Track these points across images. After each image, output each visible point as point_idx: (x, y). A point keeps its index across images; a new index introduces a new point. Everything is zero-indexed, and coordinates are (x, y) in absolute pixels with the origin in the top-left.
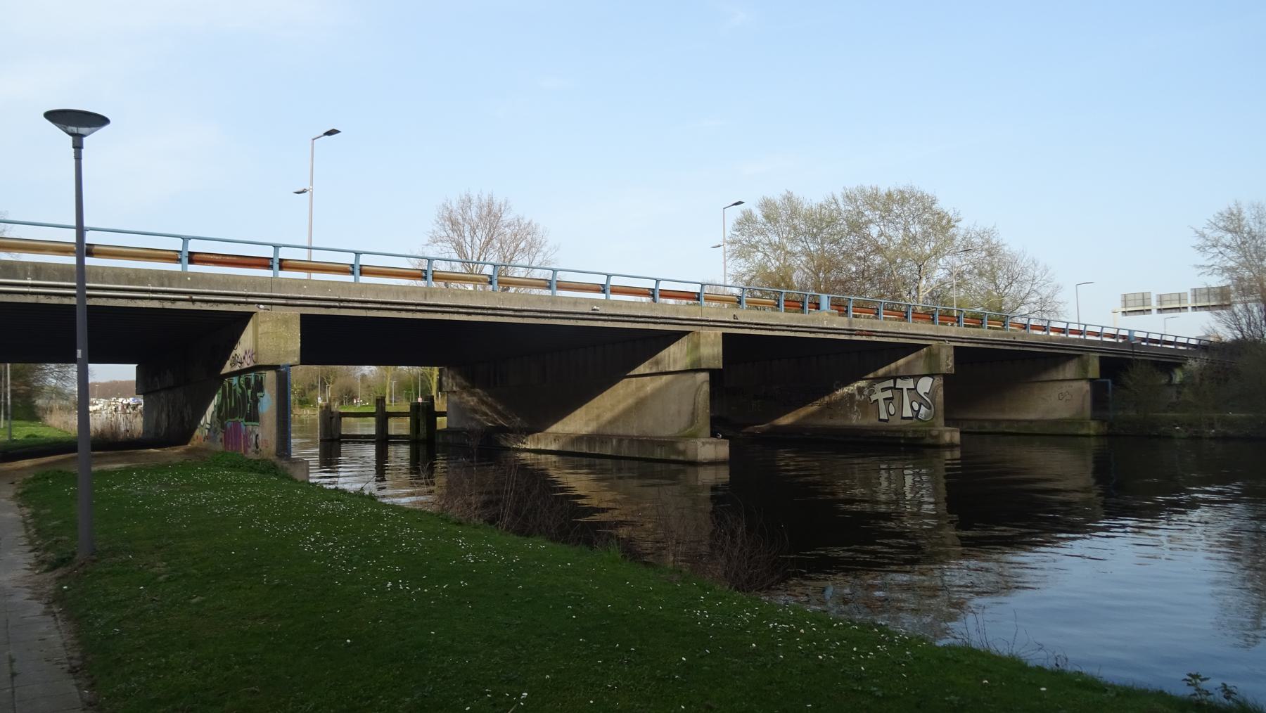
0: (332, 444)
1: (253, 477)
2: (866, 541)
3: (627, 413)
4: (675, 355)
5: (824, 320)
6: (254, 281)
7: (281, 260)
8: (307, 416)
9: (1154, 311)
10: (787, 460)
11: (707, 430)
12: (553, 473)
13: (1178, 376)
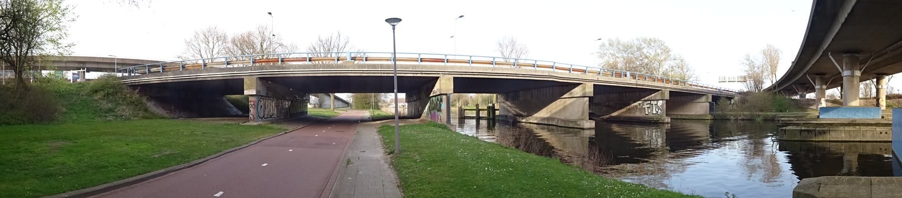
0: (462, 119)
1: (440, 130)
2: (640, 154)
3: (560, 111)
4: (577, 91)
5: (628, 81)
6: (439, 67)
8: (454, 110)
10: (615, 128)
11: (588, 118)
12: (536, 131)
13: (733, 101)
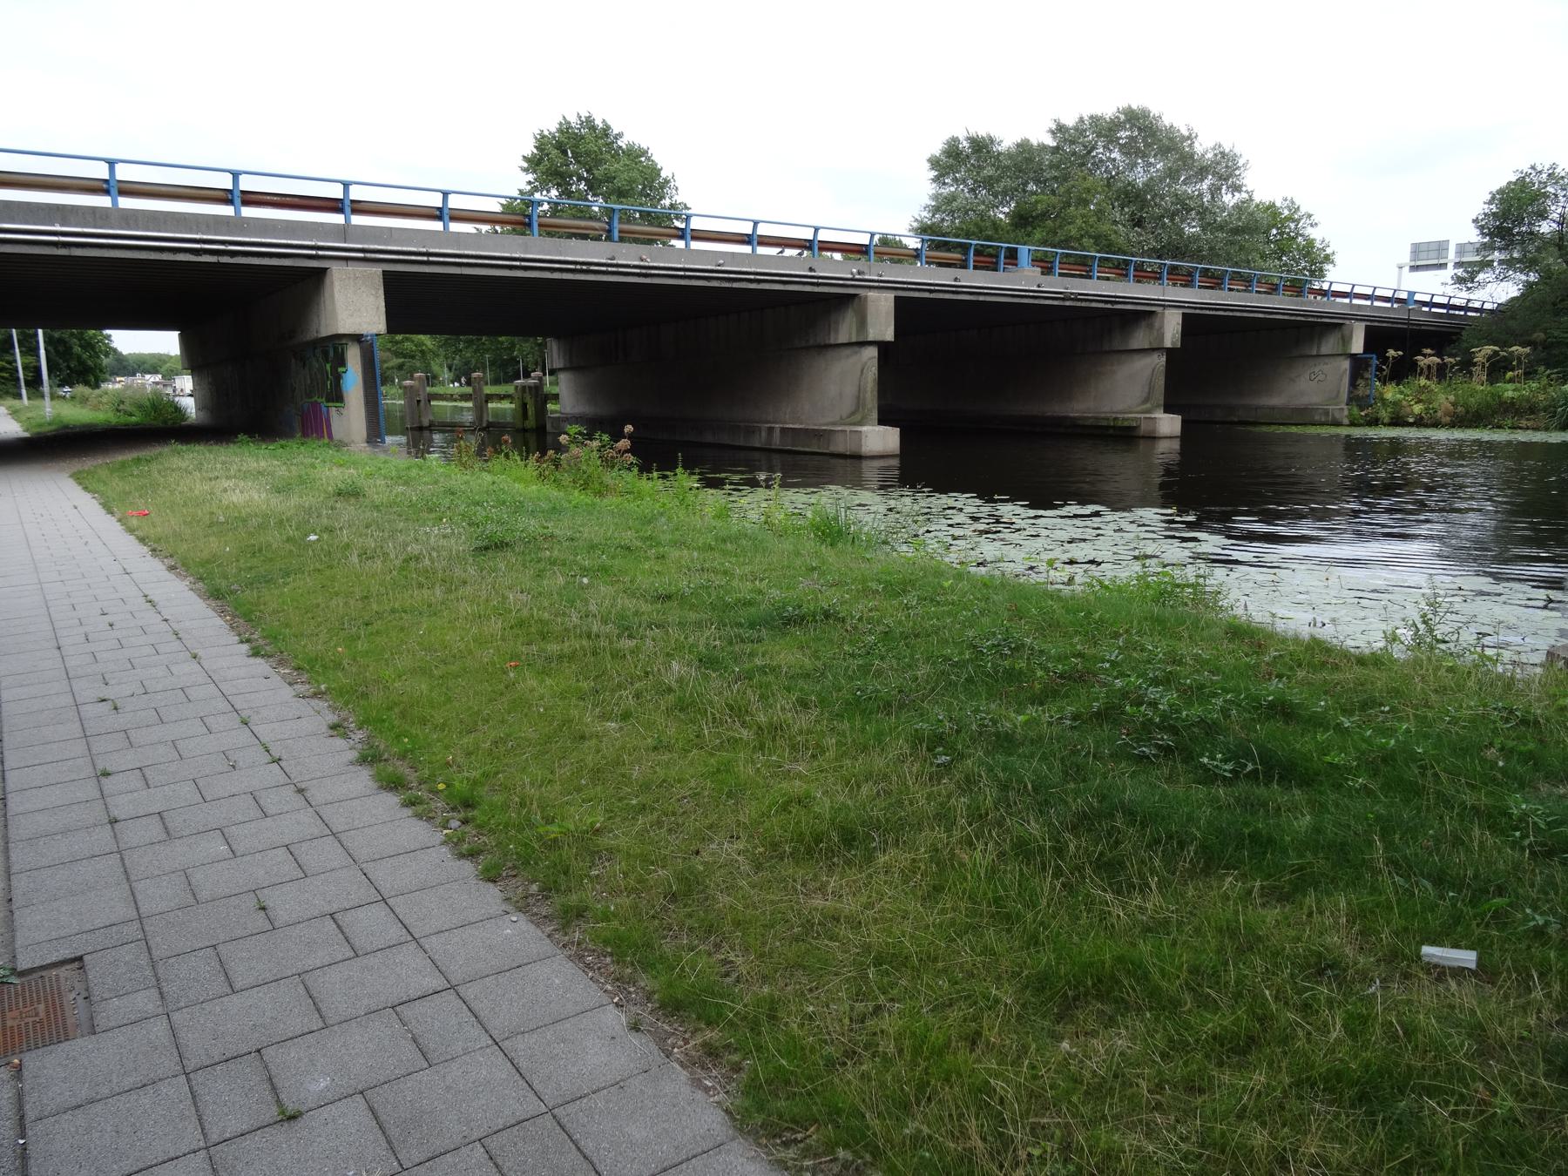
7: (353, 202)
9: (1450, 266)
11: (875, 415)
